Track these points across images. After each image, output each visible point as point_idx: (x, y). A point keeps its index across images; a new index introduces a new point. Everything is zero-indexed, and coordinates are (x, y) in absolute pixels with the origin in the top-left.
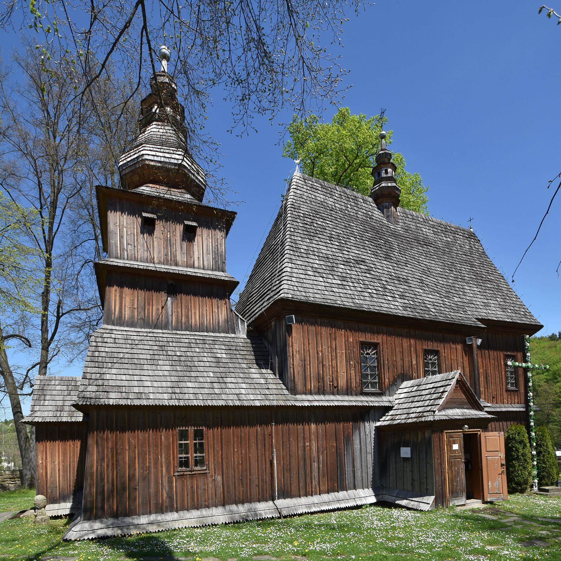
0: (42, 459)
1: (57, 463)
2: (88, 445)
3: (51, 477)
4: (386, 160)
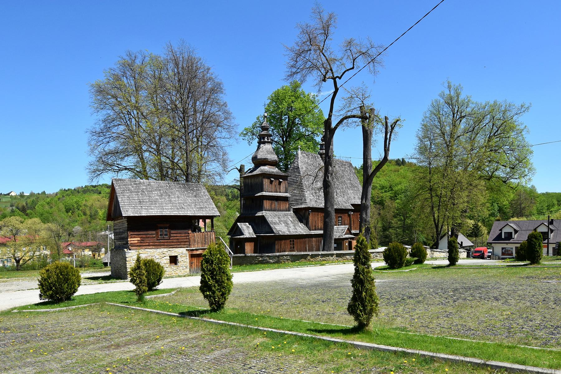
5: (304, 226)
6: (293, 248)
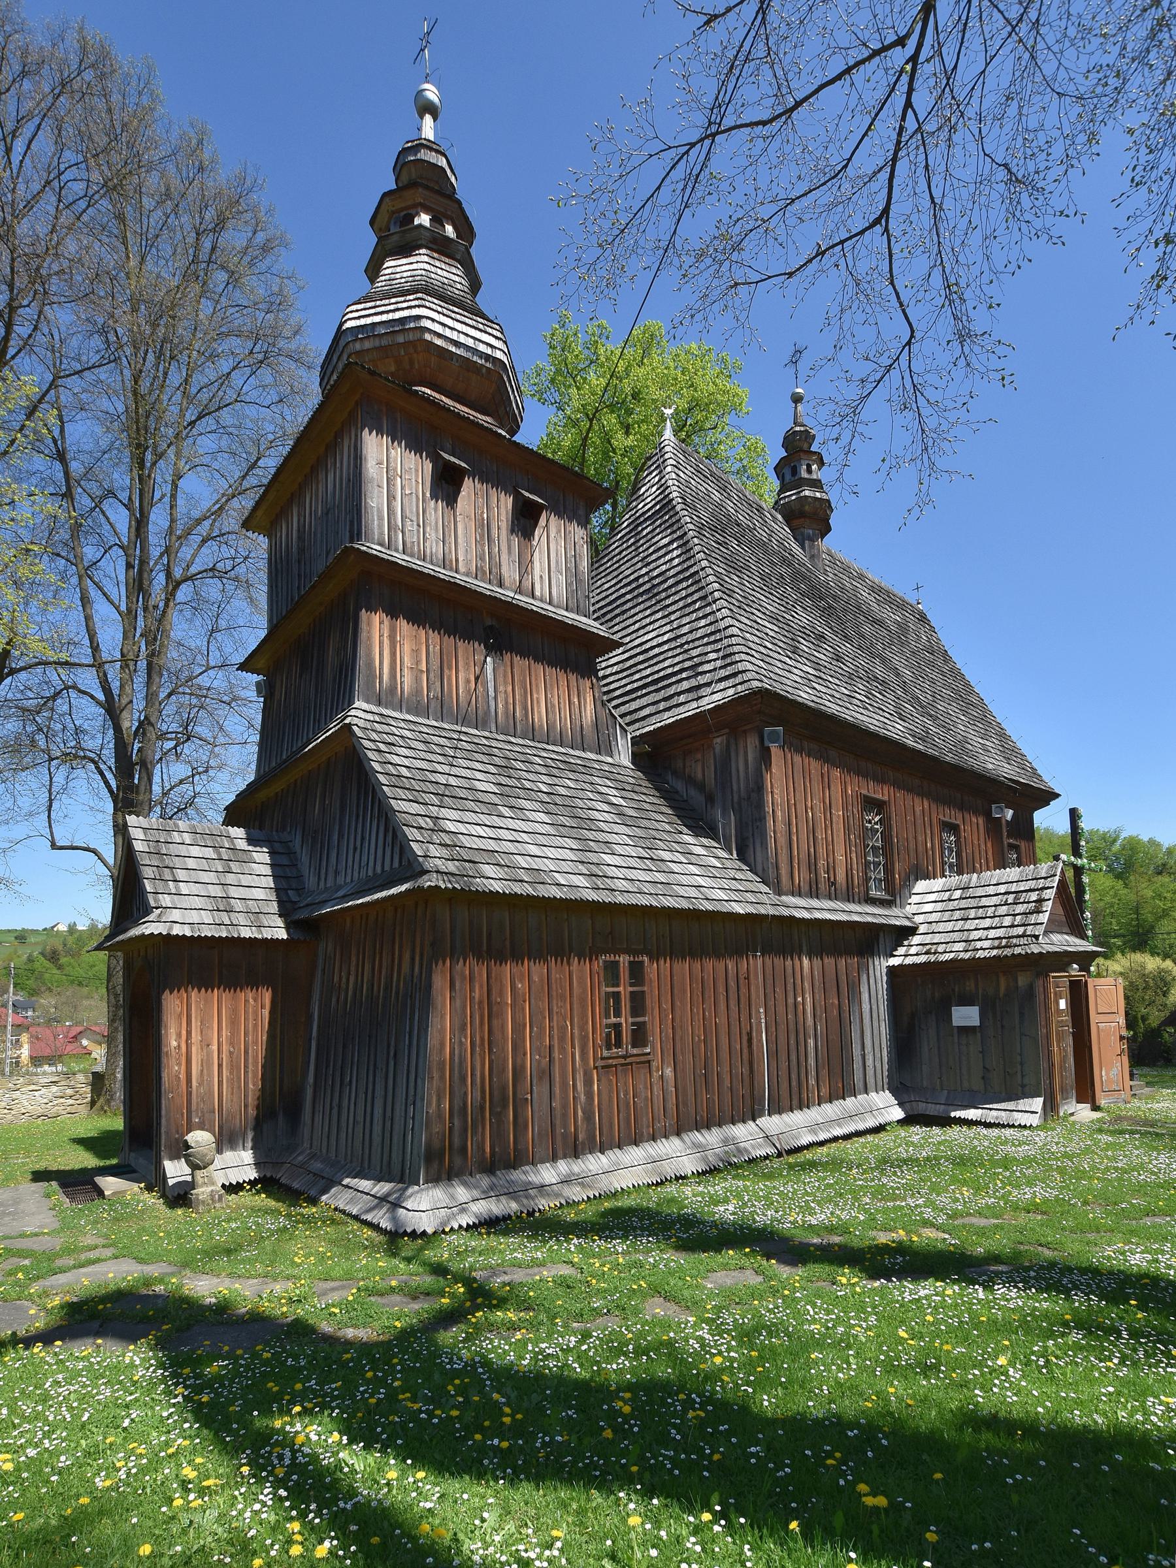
0: (179, 1035)
1: (215, 1047)
2: (434, 992)
3: (200, 1084)
4: (805, 446)
5: (722, 854)
6: (639, 1036)
